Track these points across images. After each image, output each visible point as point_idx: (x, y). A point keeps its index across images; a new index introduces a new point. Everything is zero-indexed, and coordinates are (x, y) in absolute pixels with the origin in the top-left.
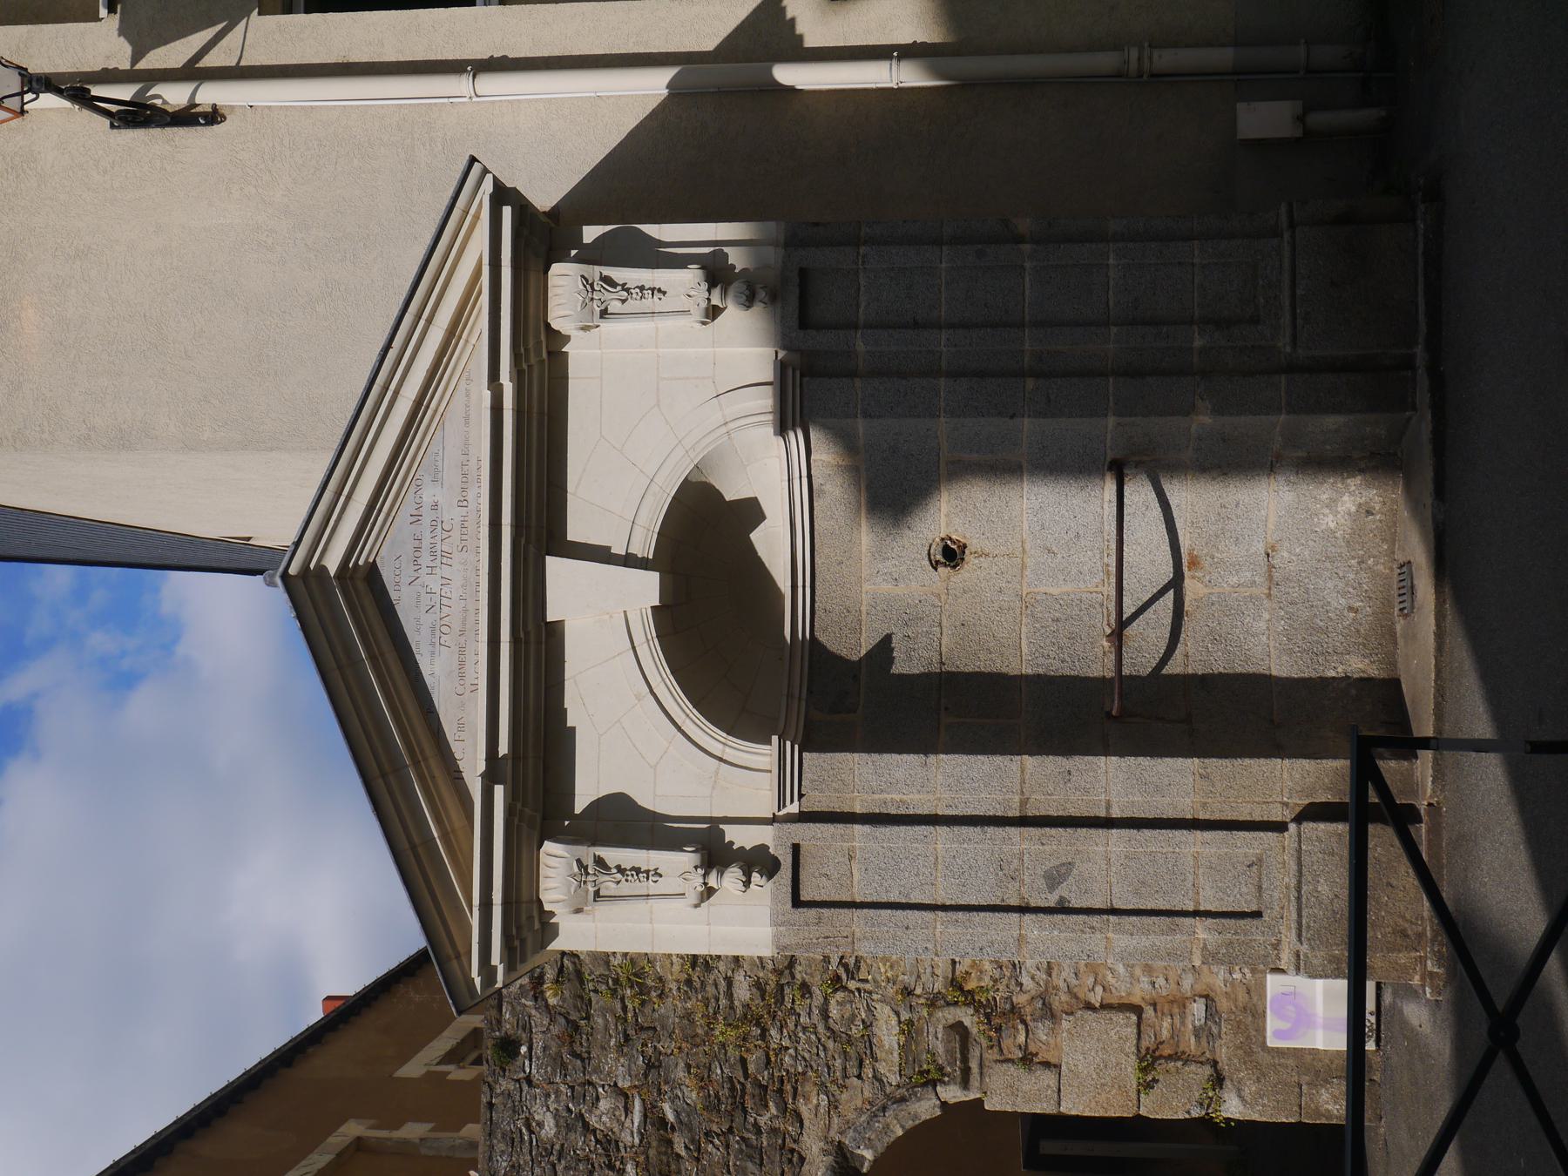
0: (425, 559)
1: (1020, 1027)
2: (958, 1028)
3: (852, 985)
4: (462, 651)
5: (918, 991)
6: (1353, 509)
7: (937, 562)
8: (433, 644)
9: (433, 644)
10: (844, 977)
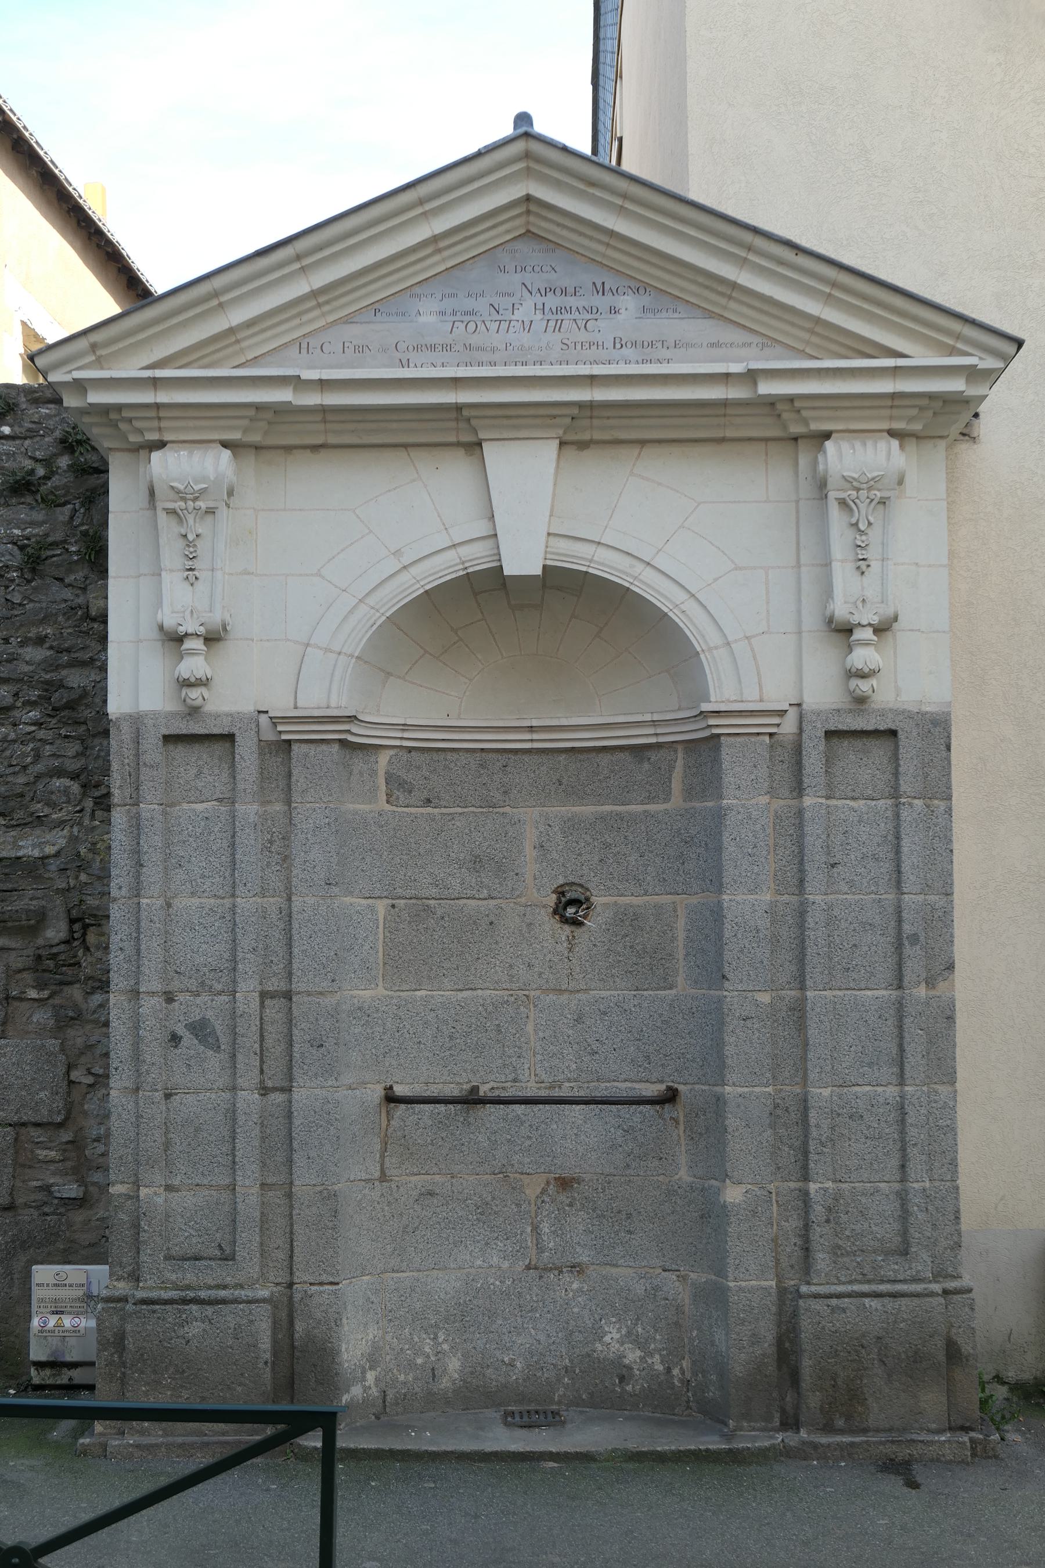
0: (552, 301)
1: (45, 994)
2: (41, 918)
3: (89, 804)
4: (447, 347)
5: (83, 877)
6: (626, 1361)
7: (563, 894)
8: (454, 313)
9: (454, 313)
10: (97, 794)
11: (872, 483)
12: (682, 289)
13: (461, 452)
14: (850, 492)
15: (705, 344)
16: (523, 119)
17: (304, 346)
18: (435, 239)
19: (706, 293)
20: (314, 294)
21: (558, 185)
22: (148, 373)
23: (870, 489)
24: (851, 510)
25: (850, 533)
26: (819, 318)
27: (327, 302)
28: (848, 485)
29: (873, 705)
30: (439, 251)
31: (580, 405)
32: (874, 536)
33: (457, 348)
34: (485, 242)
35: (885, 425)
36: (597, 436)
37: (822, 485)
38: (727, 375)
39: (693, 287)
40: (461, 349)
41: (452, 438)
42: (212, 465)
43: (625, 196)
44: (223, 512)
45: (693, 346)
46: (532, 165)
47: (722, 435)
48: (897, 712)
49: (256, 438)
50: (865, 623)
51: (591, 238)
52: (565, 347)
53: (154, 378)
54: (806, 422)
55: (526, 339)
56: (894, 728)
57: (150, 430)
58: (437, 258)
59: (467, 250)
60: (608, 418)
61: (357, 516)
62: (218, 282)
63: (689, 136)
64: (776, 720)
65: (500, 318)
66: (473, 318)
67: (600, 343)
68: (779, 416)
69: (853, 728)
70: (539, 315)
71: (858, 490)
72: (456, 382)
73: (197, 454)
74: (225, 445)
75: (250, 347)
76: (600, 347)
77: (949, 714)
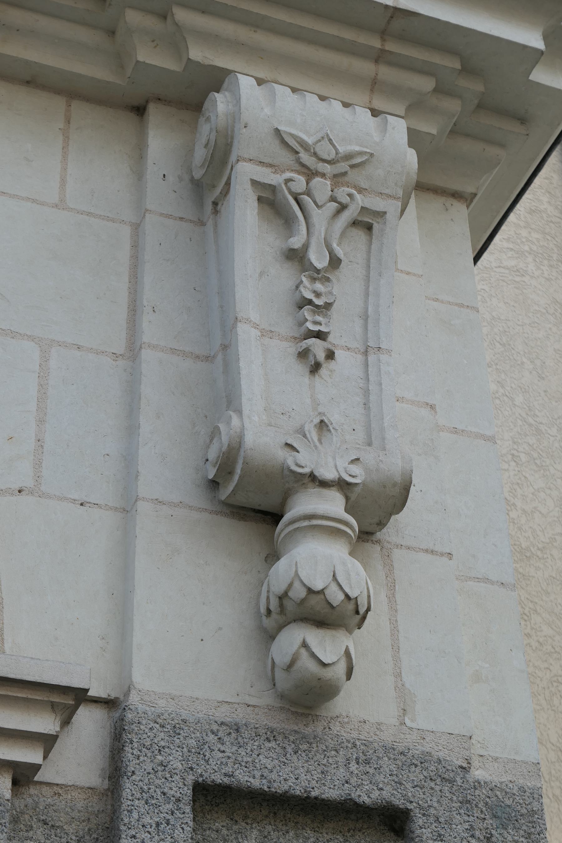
14: (288, 175)
25: (284, 277)
28: (285, 158)
29: (336, 728)
32: (345, 290)
48: (408, 760)
50: (329, 474)
56: (399, 802)
64: (43, 723)
69: (280, 787)
71: (310, 174)
77: (536, 795)
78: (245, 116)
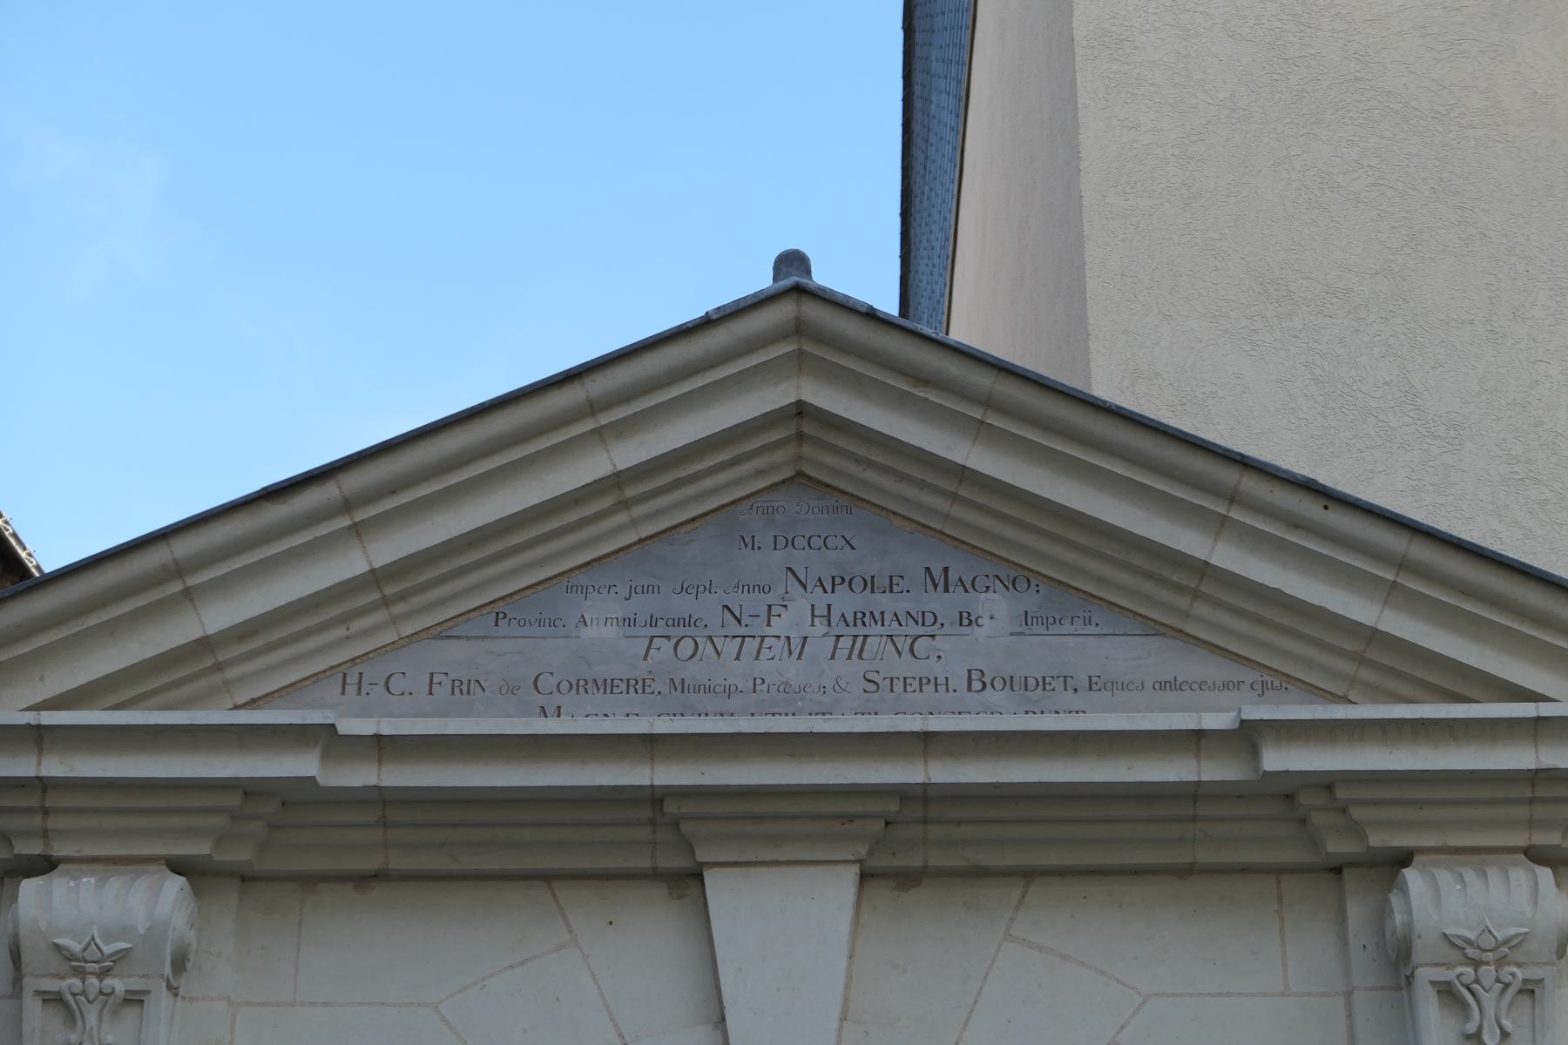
0: (846, 602)
4: (637, 685)
8: (653, 622)
9: (653, 622)
11: (1505, 950)
12: (1101, 581)
13: (659, 891)
14: (1460, 969)
15: (1149, 684)
16: (792, 262)
17: (352, 679)
18: (617, 480)
19: (1148, 587)
20: (375, 578)
21: (858, 384)
22: (29, 718)
23: (1501, 962)
24: (1465, 1006)
26: (1375, 630)
27: (402, 597)
28: (1455, 955)
30: (626, 504)
31: (903, 794)
33: (656, 687)
34: (715, 491)
35: (1519, 839)
36: (937, 859)
37: (1398, 960)
38: (1198, 736)
39: (1123, 577)
40: (665, 689)
41: (643, 862)
42: (155, 903)
43: (987, 402)
44: (161, 1003)
45: (1125, 687)
46: (808, 347)
47: (1189, 860)
49: (240, 855)
51: (922, 485)
52: (872, 687)
53: (39, 727)
54: (1358, 830)
55: (792, 670)
57: (27, 834)
58: (621, 518)
59: (679, 505)
60: (959, 823)
61: (443, 1018)
62: (183, 548)
63: (1093, 365)
65: (742, 631)
66: (691, 631)
67: (941, 680)
68: (1303, 821)
70: (820, 627)
71: (1477, 964)
72: (651, 745)
73: (115, 884)
74: (177, 867)
75: (242, 679)
76: (942, 689)
78: (1418, 927)
